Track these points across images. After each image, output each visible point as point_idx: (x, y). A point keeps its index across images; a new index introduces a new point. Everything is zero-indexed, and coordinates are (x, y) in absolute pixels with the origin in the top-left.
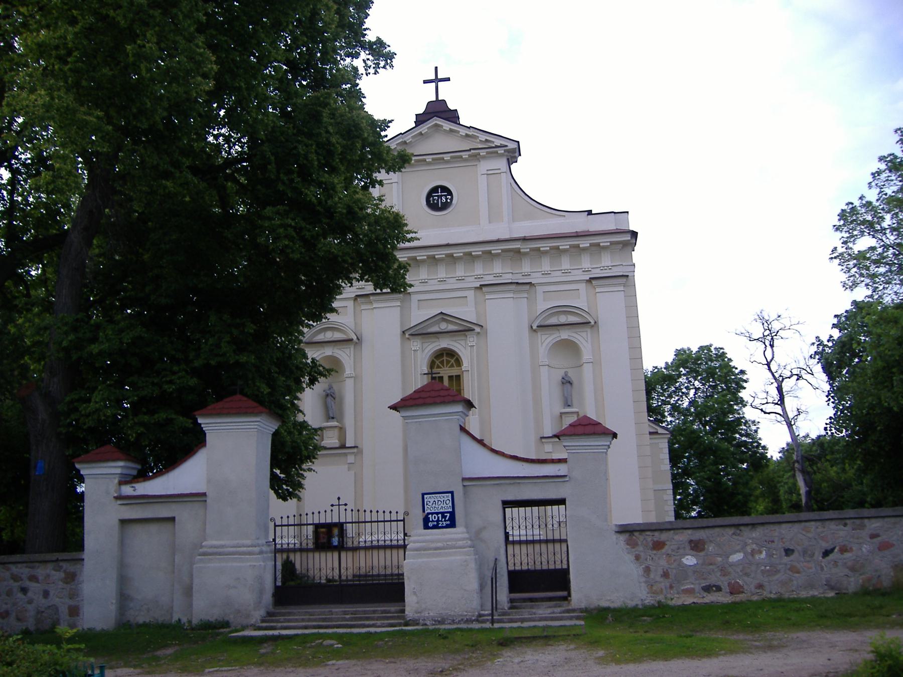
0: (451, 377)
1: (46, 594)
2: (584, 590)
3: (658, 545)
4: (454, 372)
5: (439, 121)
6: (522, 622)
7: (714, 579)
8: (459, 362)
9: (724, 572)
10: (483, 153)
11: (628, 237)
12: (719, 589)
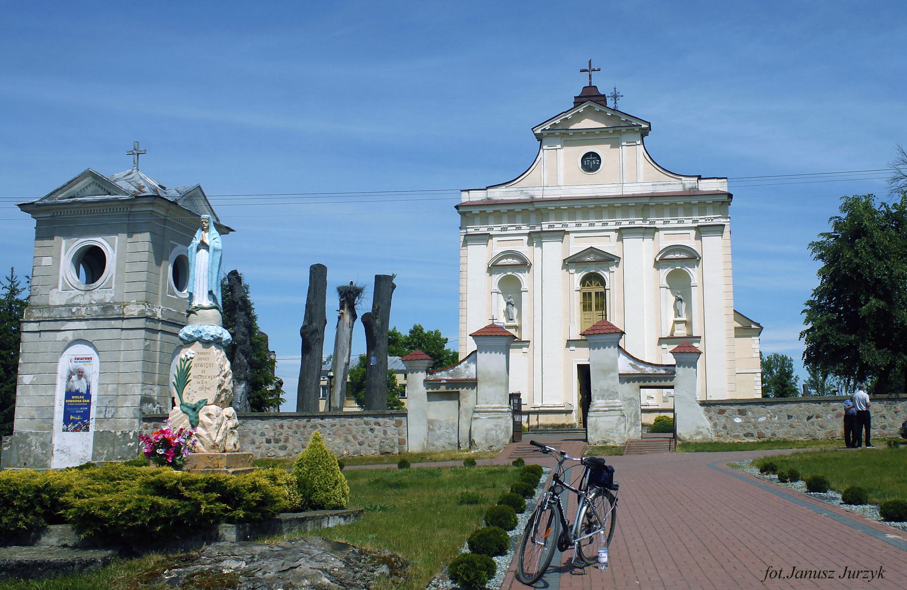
0: (597, 293)
1: (385, 432)
2: (682, 430)
3: (722, 412)
4: (601, 290)
5: (592, 104)
6: (692, 194)
7: (749, 430)
8: (603, 283)
9: (755, 427)
10: (624, 130)
11: (725, 198)
12: (752, 435)
